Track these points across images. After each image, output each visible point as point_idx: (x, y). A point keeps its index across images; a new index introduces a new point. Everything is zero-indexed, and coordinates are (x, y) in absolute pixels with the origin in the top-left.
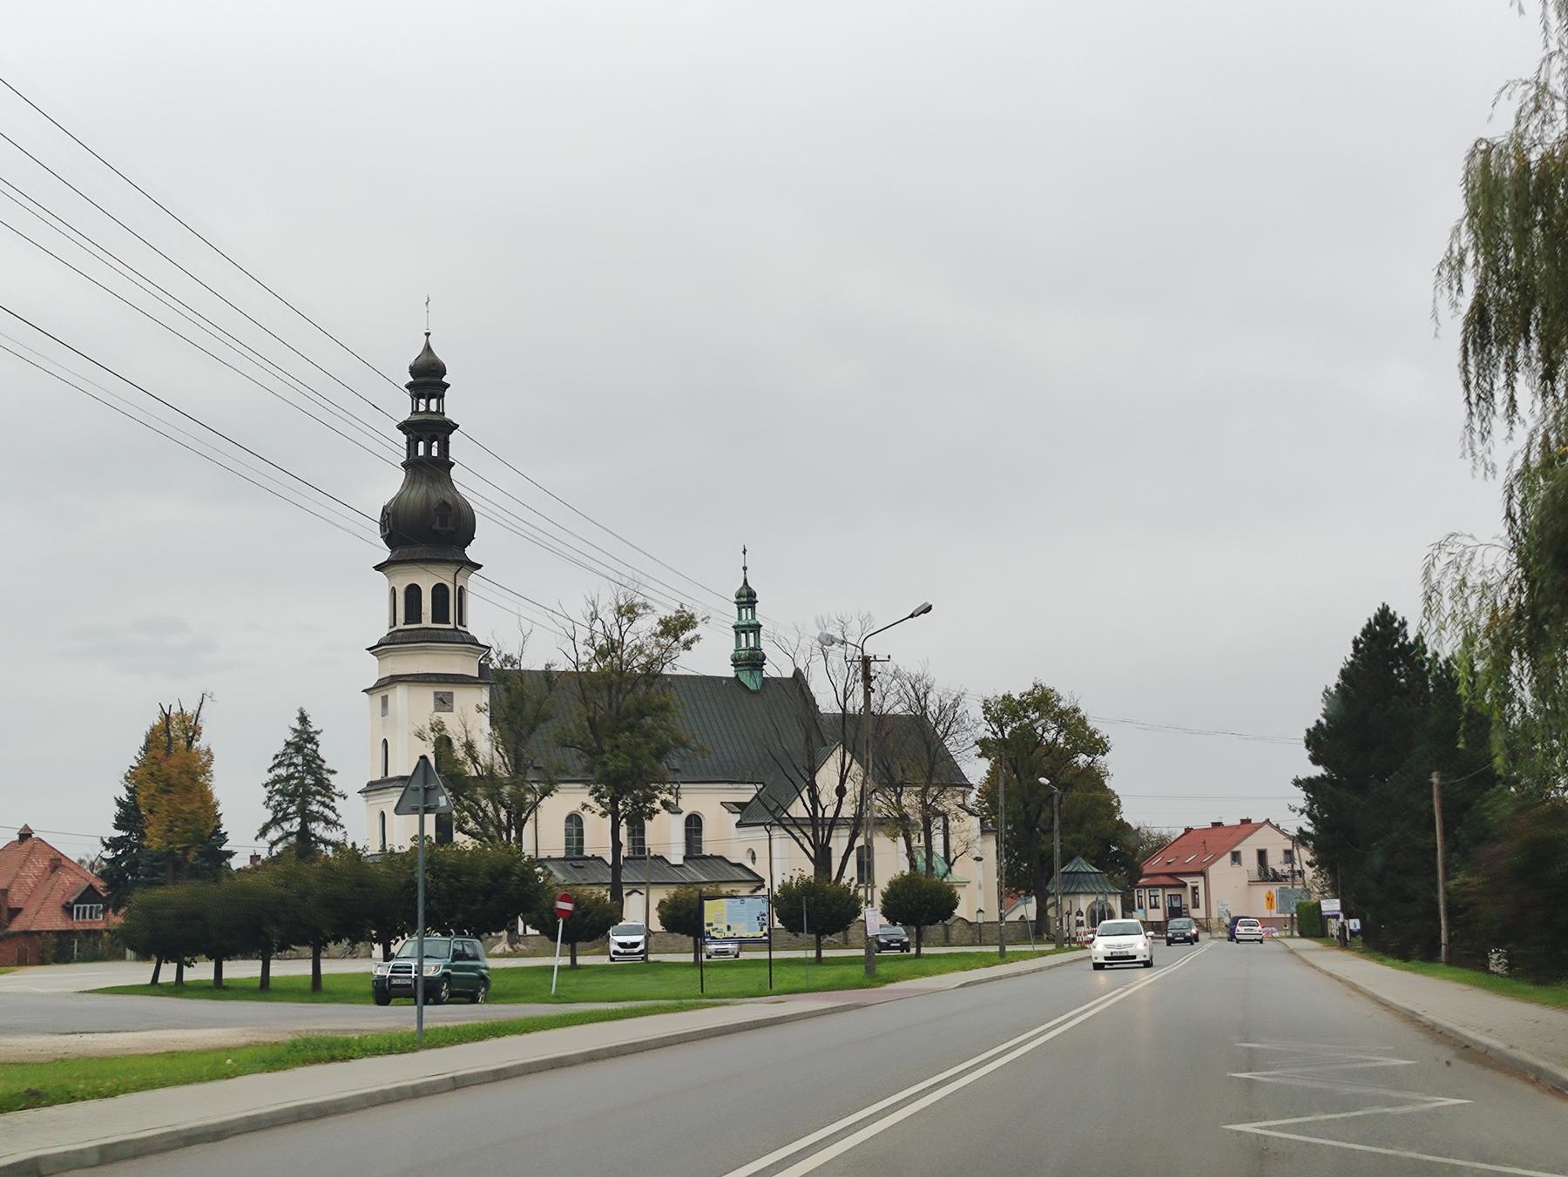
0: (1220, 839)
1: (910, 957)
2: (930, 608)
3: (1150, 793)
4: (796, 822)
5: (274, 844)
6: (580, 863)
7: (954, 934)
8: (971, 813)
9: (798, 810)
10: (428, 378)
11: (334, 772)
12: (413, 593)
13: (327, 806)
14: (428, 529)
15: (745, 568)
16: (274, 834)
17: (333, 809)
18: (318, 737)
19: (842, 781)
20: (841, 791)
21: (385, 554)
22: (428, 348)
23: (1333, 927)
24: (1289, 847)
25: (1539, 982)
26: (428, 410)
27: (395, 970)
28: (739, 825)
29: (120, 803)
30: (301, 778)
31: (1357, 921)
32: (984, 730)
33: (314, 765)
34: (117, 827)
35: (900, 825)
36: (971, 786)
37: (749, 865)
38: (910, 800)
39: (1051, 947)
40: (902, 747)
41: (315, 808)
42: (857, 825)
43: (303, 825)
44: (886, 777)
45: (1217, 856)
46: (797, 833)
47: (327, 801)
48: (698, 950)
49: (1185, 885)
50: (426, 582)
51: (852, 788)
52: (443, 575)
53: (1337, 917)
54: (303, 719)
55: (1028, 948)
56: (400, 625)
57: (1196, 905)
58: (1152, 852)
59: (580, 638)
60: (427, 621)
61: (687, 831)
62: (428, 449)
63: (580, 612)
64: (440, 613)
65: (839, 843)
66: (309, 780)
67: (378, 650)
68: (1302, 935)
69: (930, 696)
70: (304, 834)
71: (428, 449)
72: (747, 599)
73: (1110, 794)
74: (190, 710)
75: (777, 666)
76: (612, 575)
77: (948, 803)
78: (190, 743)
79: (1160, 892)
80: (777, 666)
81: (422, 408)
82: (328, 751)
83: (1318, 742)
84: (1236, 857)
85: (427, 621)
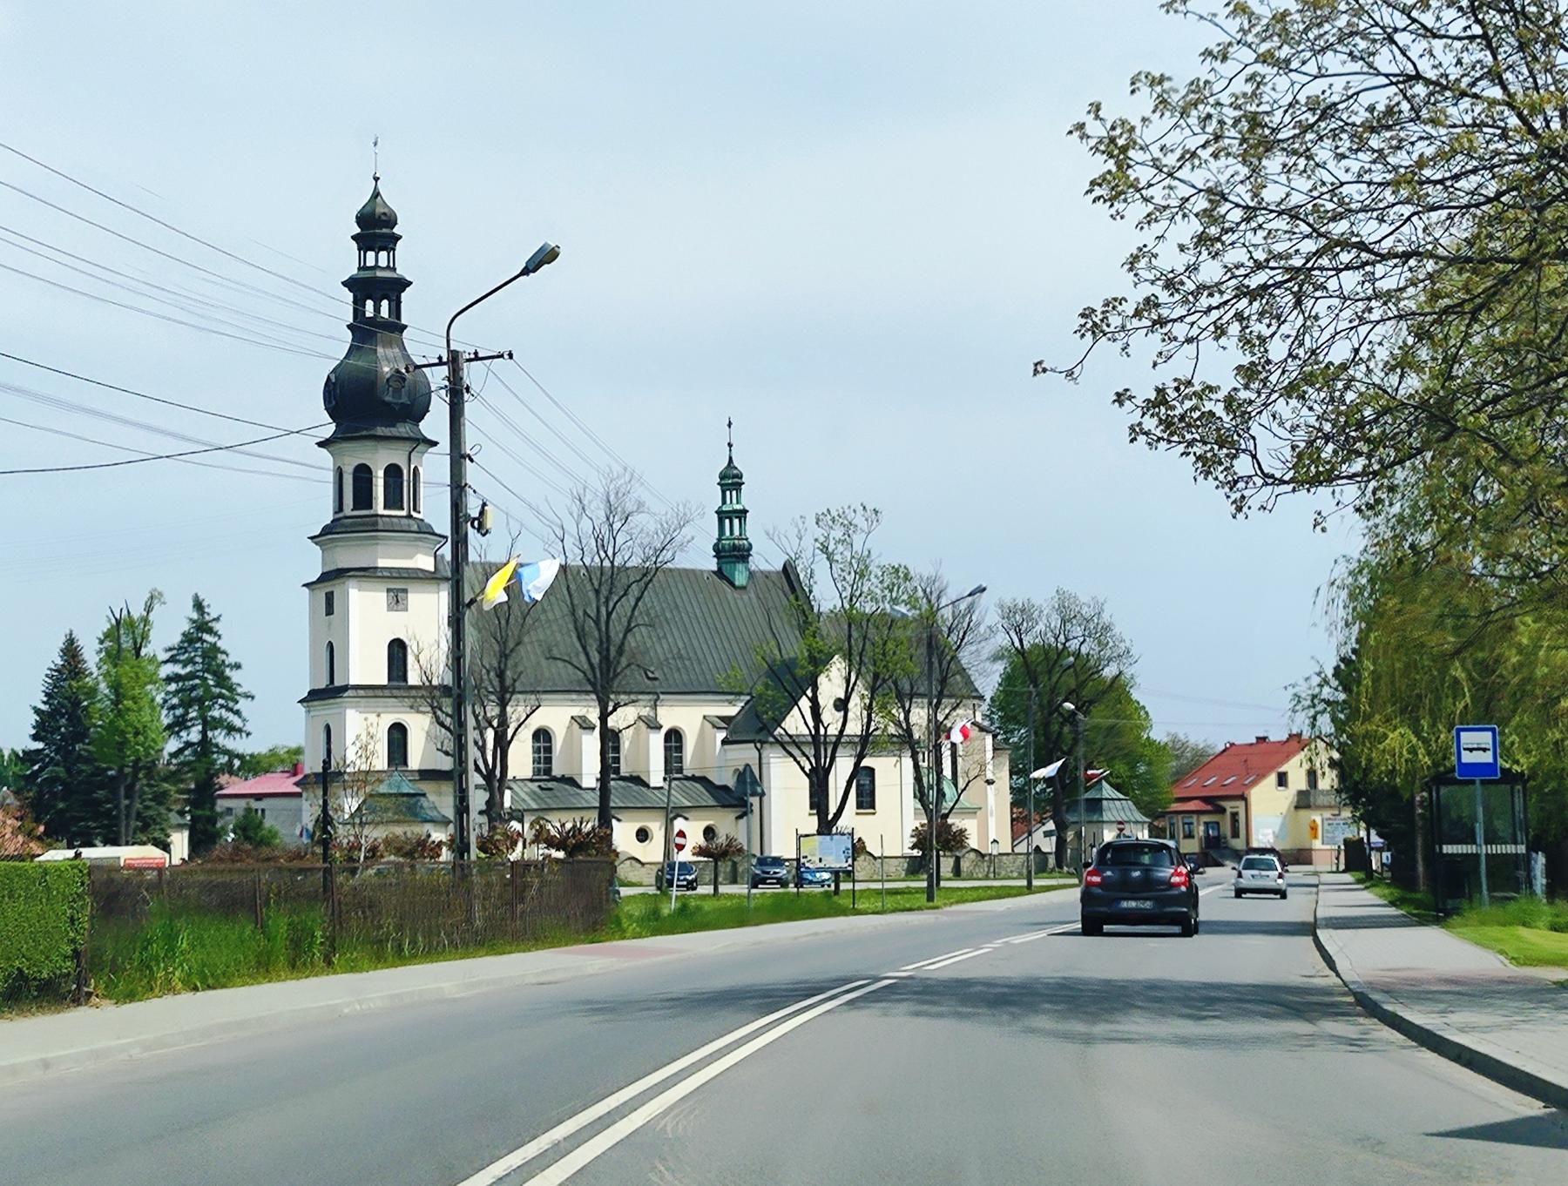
4: (795, 741)
6: (550, 785)
7: (965, 865)
8: (982, 729)
9: (796, 723)
11: (238, 666)
12: (363, 475)
13: (231, 710)
14: (369, 404)
15: (730, 445)
17: (237, 713)
18: (216, 626)
20: (842, 705)
21: (330, 430)
22: (376, 194)
28: (724, 742)
29: (37, 711)
34: (35, 738)
35: (906, 741)
36: (981, 698)
38: (919, 716)
40: (909, 655)
41: (216, 713)
42: (865, 744)
43: (204, 733)
44: (886, 687)
45: (1261, 776)
46: (796, 752)
47: (231, 704)
49: (1223, 811)
50: (379, 460)
51: (855, 705)
54: (199, 606)
57: (1236, 834)
61: (666, 748)
62: (377, 309)
64: (393, 500)
65: (843, 767)
70: (205, 741)
71: (377, 309)
75: (766, 558)
77: (960, 719)
79: (1194, 819)
80: (766, 558)
82: (231, 641)
84: (1282, 780)
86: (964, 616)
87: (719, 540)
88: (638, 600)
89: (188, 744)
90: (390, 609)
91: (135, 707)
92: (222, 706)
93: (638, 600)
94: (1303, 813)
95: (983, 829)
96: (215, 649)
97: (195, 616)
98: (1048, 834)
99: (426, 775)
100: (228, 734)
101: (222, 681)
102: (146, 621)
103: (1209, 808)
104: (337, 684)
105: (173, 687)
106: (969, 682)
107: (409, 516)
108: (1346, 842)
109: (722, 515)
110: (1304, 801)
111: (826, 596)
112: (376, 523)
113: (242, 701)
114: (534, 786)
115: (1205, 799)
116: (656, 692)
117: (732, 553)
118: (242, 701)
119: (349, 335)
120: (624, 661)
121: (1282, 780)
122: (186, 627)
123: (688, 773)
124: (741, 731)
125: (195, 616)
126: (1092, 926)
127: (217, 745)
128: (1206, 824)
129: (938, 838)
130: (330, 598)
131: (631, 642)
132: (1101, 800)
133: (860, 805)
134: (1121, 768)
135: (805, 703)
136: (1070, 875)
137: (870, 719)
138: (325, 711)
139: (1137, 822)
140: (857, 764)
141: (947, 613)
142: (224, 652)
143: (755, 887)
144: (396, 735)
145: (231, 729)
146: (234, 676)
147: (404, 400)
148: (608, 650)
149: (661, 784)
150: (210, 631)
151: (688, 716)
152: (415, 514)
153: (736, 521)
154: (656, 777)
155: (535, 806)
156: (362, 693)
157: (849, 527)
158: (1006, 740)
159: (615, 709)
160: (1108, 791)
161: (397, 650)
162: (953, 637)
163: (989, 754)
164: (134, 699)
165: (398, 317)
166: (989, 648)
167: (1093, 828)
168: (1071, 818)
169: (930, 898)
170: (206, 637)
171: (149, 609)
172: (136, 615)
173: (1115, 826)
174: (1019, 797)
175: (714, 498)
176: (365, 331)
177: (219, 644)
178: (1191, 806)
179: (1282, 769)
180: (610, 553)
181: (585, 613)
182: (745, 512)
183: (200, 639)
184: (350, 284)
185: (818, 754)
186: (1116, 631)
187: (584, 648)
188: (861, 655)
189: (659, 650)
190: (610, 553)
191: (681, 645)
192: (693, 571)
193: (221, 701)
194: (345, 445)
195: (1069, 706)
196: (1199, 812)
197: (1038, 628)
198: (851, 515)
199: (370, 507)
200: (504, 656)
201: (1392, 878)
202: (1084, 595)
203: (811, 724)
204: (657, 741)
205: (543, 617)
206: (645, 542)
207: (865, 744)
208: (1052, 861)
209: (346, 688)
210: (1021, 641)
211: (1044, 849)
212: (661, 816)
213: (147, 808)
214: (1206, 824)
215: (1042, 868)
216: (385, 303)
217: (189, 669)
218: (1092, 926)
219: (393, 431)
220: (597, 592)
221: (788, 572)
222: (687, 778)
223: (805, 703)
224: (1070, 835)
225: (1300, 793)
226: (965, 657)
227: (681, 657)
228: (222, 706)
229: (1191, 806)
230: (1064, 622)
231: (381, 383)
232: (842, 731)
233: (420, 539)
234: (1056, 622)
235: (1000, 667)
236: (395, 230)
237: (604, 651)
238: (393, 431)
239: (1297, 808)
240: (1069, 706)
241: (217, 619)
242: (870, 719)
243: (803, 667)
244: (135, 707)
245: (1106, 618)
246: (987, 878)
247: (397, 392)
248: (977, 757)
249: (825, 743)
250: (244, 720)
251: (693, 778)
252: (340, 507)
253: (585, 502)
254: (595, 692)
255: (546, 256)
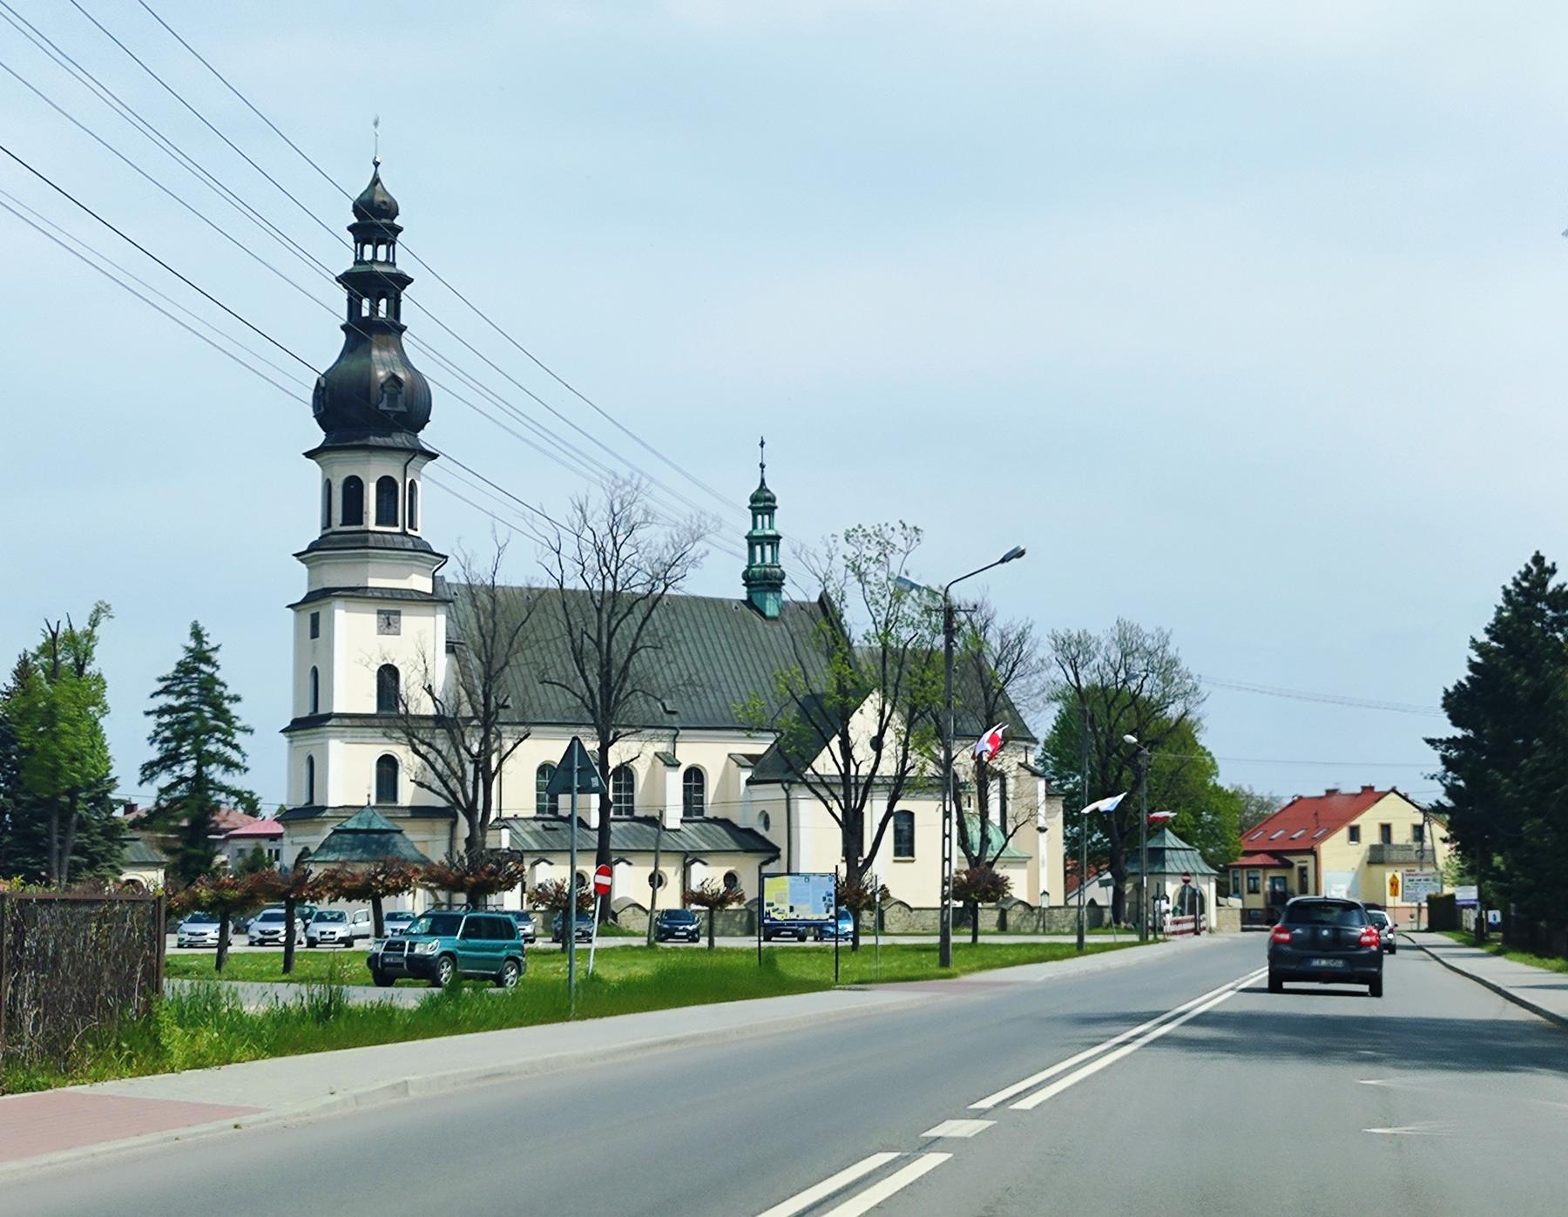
0: (1332, 811)
1: (701, 950)
2: (1023, 553)
3: (1253, 751)
4: (823, 782)
5: (162, 791)
6: (555, 824)
7: (1012, 919)
8: (1035, 774)
9: (826, 764)
10: (375, 219)
11: (237, 699)
12: (354, 488)
13: (226, 743)
14: (368, 410)
15: (762, 466)
16: (164, 779)
17: (236, 747)
18: (215, 656)
19: (882, 733)
20: (877, 744)
21: (318, 437)
22: (376, 180)
23: (1469, 918)
24: (1420, 822)
25: (1540, 956)
26: (374, 260)
27: (391, 946)
28: (749, 782)
30: (196, 708)
31: (1498, 913)
33: (210, 694)
36: (1035, 741)
37: (761, 831)
39: (1135, 938)
40: (950, 682)
42: (899, 786)
43: (198, 768)
45: (1331, 831)
46: (824, 792)
48: (975, 935)
49: (1290, 865)
50: (371, 472)
52: (389, 467)
53: (1473, 907)
54: (197, 634)
55: (1121, 938)
58: (1245, 828)
59: (570, 549)
60: (371, 523)
62: (374, 309)
63: (564, 513)
64: (387, 514)
65: (875, 810)
66: (207, 711)
67: (311, 555)
68: (1431, 929)
69: (990, 631)
71: (374, 309)
72: (763, 504)
73: (1205, 752)
74: (80, 626)
75: (800, 588)
77: (1009, 761)
78: (80, 668)
79: (1260, 874)
80: (800, 588)
81: (368, 256)
82: (230, 672)
83: (1457, 704)
84: (1354, 834)
85: (371, 523)
86: (1013, 647)
87: (749, 567)
88: (645, 620)
89: (182, 779)
90: (381, 632)
91: (71, 730)
92: (218, 740)
93: (645, 620)
94: (1376, 869)
95: (1034, 880)
96: (212, 679)
97: (192, 644)
98: (1104, 884)
99: (419, 812)
100: (227, 770)
101: (221, 714)
102: (89, 636)
103: (1276, 862)
104: (321, 711)
105: (166, 719)
106: (1017, 719)
107: (405, 533)
108: (1430, 899)
109: (753, 541)
110: (1377, 857)
111: (859, 622)
112: (367, 540)
113: (238, 734)
114: (538, 825)
115: (1271, 853)
116: (673, 725)
117: (763, 582)
118: (238, 734)
119: (342, 336)
120: (628, 686)
121: (1354, 834)
122: (181, 656)
123: (709, 813)
124: (761, 771)
125: (192, 644)
127: (212, 781)
128: (1273, 879)
129: (976, 887)
130: (315, 619)
131: (636, 666)
132: (1163, 850)
133: (898, 852)
134: (1187, 817)
135: (835, 743)
136: (1128, 931)
137: (905, 757)
138: (308, 742)
139: (1203, 874)
140: (891, 806)
141: (995, 643)
142: (222, 684)
143: (768, 939)
144: (387, 768)
145: (229, 765)
146: (234, 709)
147: (401, 408)
148: (608, 673)
149: (677, 825)
150: (208, 661)
151: (712, 755)
152: (410, 532)
153: (768, 548)
154: (673, 818)
155: (536, 847)
156: (347, 722)
157: (885, 546)
158: (1060, 786)
159: (615, 740)
160: (1171, 839)
161: (388, 677)
162: (1002, 669)
163: (1042, 796)
164: (72, 722)
165: (397, 315)
166: (1038, 682)
167: (1155, 879)
168: (1130, 869)
169: (945, 962)
170: (203, 667)
171: (94, 623)
172: (78, 630)
173: (1180, 879)
174: (1073, 848)
175: (744, 523)
176: (361, 333)
177: (217, 675)
178: (1258, 860)
179: (1354, 823)
180: (613, 568)
181: (583, 632)
182: (778, 538)
183: (197, 670)
184: (346, 279)
185: (849, 795)
186: (1183, 666)
187: (582, 672)
188: (896, 686)
189: (669, 677)
190: (613, 568)
191: (692, 670)
192: (721, 601)
193: (218, 735)
194: (333, 455)
195: (1131, 739)
196: (1265, 867)
197: (1095, 662)
198: (888, 534)
199: (361, 523)
200: (489, 678)
201: (1505, 940)
202: (1148, 625)
203: (840, 761)
204: (674, 782)
205: (532, 637)
206: (656, 555)
207: (899, 786)
208: (1108, 915)
209: (330, 716)
210: (1076, 675)
211: (1099, 903)
212: (678, 860)
213: (95, 843)
214: (1273, 879)
215: (1097, 923)
216: (383, 302)
217: (183, 700)
219: (388, 441)
220: (599, 610)
221: (824, 602)
222: (708, 820)
223: (835, 743)
224: (1128, 887)
225: (1373, 847)
226: (1014, 691)
227: (692, 684)
228: (218, 740)
229: (1258, 860)
230: (1125, 655)
231: (375, 390)
232: (874, 769)
233: (415, 558)
234: (1115, 655)
235: (1055, 709)
236: (396, 221)
237: (605, 676)
238: (388, 441)
239: (1370, 863)
240: (1131, 739)
241: (215, 649)
242: (905, 757)
243: (831, 698)
244: (71, 730)
245: (1171, 651)
246: (1035, 932)
247: (393, 399)
248: (1026, 801)
249: (857, 784)
250: (244, 755)
251: (715, 821)
252: (328, 522)
253: (588, 514)
254: (595, 725)
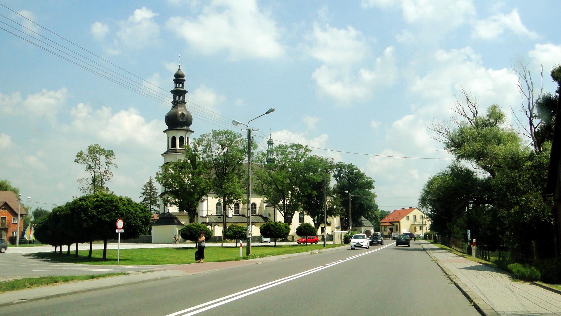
3: (384, 199)
10: (179, 78)
12: (174, 139)
21: (166, 127)
22: (179, 69)
32: (32, 219)
45: (402, 217)
49: (394, 225)
50: (178, 135)
56: (170, 148)
60: (178, 147)
76: (519, 124)
84: (408, 218)
126: (397, 246)
176: (176, 104)
184: (172, 92)
218: (397, 246)
247: (183, 119)
251: (258, 215)
255: (272, 111)
